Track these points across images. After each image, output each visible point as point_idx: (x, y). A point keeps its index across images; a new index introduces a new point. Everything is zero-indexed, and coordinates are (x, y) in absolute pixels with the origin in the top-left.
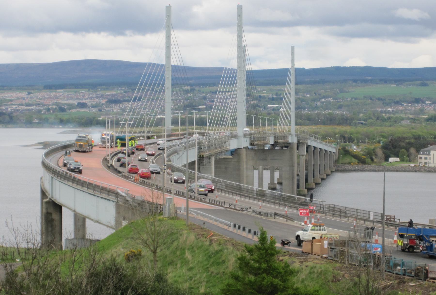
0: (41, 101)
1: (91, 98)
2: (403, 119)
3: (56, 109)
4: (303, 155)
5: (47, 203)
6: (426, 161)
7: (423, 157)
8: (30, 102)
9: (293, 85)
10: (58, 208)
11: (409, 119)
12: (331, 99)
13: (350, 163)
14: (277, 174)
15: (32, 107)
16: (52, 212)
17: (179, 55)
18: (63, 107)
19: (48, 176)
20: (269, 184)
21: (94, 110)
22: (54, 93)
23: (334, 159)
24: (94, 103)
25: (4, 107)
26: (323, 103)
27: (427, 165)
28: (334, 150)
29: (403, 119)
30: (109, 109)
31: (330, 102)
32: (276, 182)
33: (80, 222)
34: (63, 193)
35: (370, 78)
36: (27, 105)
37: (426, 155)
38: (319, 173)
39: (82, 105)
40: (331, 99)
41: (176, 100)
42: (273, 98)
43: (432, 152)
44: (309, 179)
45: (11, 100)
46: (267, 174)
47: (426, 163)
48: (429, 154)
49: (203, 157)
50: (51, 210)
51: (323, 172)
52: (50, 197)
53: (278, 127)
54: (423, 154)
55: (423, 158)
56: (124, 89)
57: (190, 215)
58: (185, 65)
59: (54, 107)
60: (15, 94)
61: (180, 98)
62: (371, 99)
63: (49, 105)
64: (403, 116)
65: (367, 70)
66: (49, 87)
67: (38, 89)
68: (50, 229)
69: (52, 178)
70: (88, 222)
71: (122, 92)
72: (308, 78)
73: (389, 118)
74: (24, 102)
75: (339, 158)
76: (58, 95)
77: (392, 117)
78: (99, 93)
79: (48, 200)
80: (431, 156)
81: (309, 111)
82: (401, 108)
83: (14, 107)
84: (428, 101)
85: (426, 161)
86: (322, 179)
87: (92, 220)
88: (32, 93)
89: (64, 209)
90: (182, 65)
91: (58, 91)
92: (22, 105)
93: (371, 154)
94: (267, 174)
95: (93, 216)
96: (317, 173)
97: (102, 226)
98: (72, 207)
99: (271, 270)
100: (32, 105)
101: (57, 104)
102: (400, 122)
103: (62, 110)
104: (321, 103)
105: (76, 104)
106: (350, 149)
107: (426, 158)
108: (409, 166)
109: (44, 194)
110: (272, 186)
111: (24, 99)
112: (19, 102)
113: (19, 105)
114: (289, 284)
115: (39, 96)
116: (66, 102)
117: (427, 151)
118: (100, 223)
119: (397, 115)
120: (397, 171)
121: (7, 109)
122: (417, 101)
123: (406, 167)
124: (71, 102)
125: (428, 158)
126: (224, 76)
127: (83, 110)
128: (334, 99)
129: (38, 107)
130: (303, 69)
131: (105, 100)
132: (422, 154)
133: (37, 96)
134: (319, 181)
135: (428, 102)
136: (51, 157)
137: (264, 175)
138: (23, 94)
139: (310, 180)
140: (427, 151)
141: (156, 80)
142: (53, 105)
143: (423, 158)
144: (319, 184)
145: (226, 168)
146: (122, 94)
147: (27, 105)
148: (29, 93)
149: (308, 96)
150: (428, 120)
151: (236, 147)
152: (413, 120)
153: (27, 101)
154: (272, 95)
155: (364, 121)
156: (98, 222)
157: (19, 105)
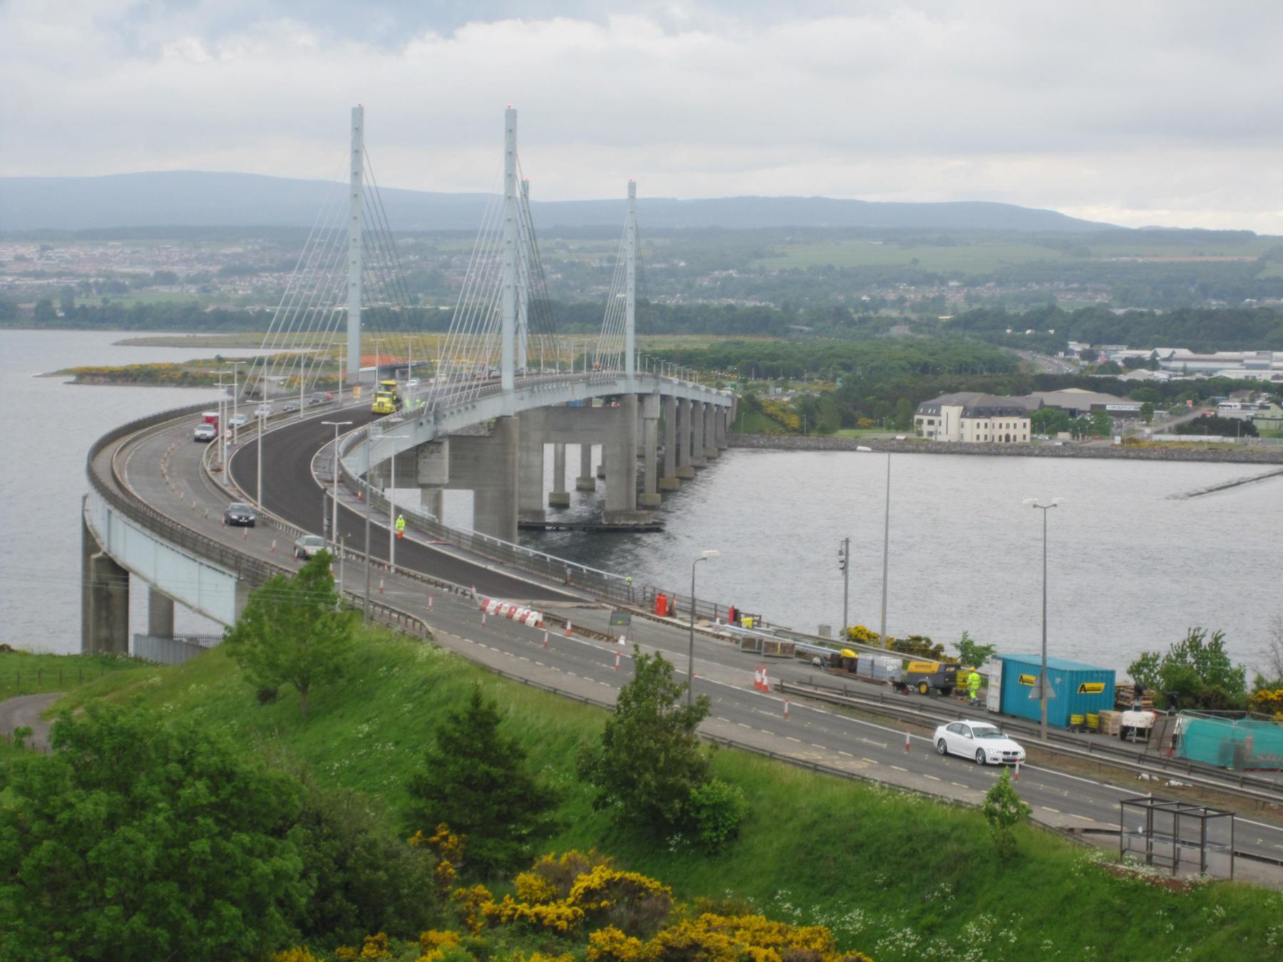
1: (186, 261)
2: (893, 322)
4: (653, 419)
5: (98, 560)
6: (931, 428)
7: (926, 419)
10: (122, 574)
11: (907, 321)
12: (733, 273)
14: (597, 453)
16: (106, 583)
18: (121, 281)
19: (98, 507)
20: (578, 479)
21: (193, 290)
22: (101, 250)
23: (728, 423)
24: (193, 272)
27: (933, 438)
30: (229, 287)
31: (730, 275)
32: (594, 474)
33: (163, 606)
34: (133, 547)
36: (38, 275)
37: (931, 414)
38: (692, 454)
39: (168, 279)
40: (733, 273)
41: (381, 269)
44: (667, 469)
46: (573, 452)
47: (931, 434)
48: (938, 414)
50: (106, 575)
51: (699, 451)
52: (104, 548)
54: (925, 413)
55: (925, 422)
56: (261, 240)
61: (390, 264)
63: (88, 276)
64: (894, 314)
68: (104, 614)
69: (110, 512)
70: (177, 607)
71: (257, 248)
73: (863, 321)
74: (31, 269)
75: (738, 419)
76: (110, 252)
77: (870, 319)
78: (205, 251)
79: (100, 554)
80: (943, 418)
83: (10, 279)
84: (953, 279)
85: (931, 428)
87: (190, 607)
89: (132, 578)
91: (111, 243)
94: (573, 452)
95: (192, 600)
96: (685, 450)
97: (209, 621)
98: (150, 575)
99: (490, 753)
100: (51, 276)
101: (109, 275)
103: (119, 289)
105: (152, 274)
106: (761, 397)
107: (931, 423)
109: (90, 542)
110: (586, 484)
114: (518, 773)
115: (67, 256)
118: (205, 615)
119: (884, 312)
122: (930, 279)
123: (886, 441)
124: (139, 270)
125: (936, 423)
126: (459, 311)
128: (740, 272)
129: (65, 281)
131: (219, 267)
132: (924, 414)
135: (953, 284)
137: (567, 456)
138: (30, 250)
139: (670, 471)
140: (932, 406)
142: (99, 276)
143: (925, 422)
147: (38, 275)
148: (44, 248)
149: (682, 264)
150: (951, 325)
151: (498, 414)
152: (916, 326)
154: (601, 260)
155: (807, 325)
156: (200, 612)
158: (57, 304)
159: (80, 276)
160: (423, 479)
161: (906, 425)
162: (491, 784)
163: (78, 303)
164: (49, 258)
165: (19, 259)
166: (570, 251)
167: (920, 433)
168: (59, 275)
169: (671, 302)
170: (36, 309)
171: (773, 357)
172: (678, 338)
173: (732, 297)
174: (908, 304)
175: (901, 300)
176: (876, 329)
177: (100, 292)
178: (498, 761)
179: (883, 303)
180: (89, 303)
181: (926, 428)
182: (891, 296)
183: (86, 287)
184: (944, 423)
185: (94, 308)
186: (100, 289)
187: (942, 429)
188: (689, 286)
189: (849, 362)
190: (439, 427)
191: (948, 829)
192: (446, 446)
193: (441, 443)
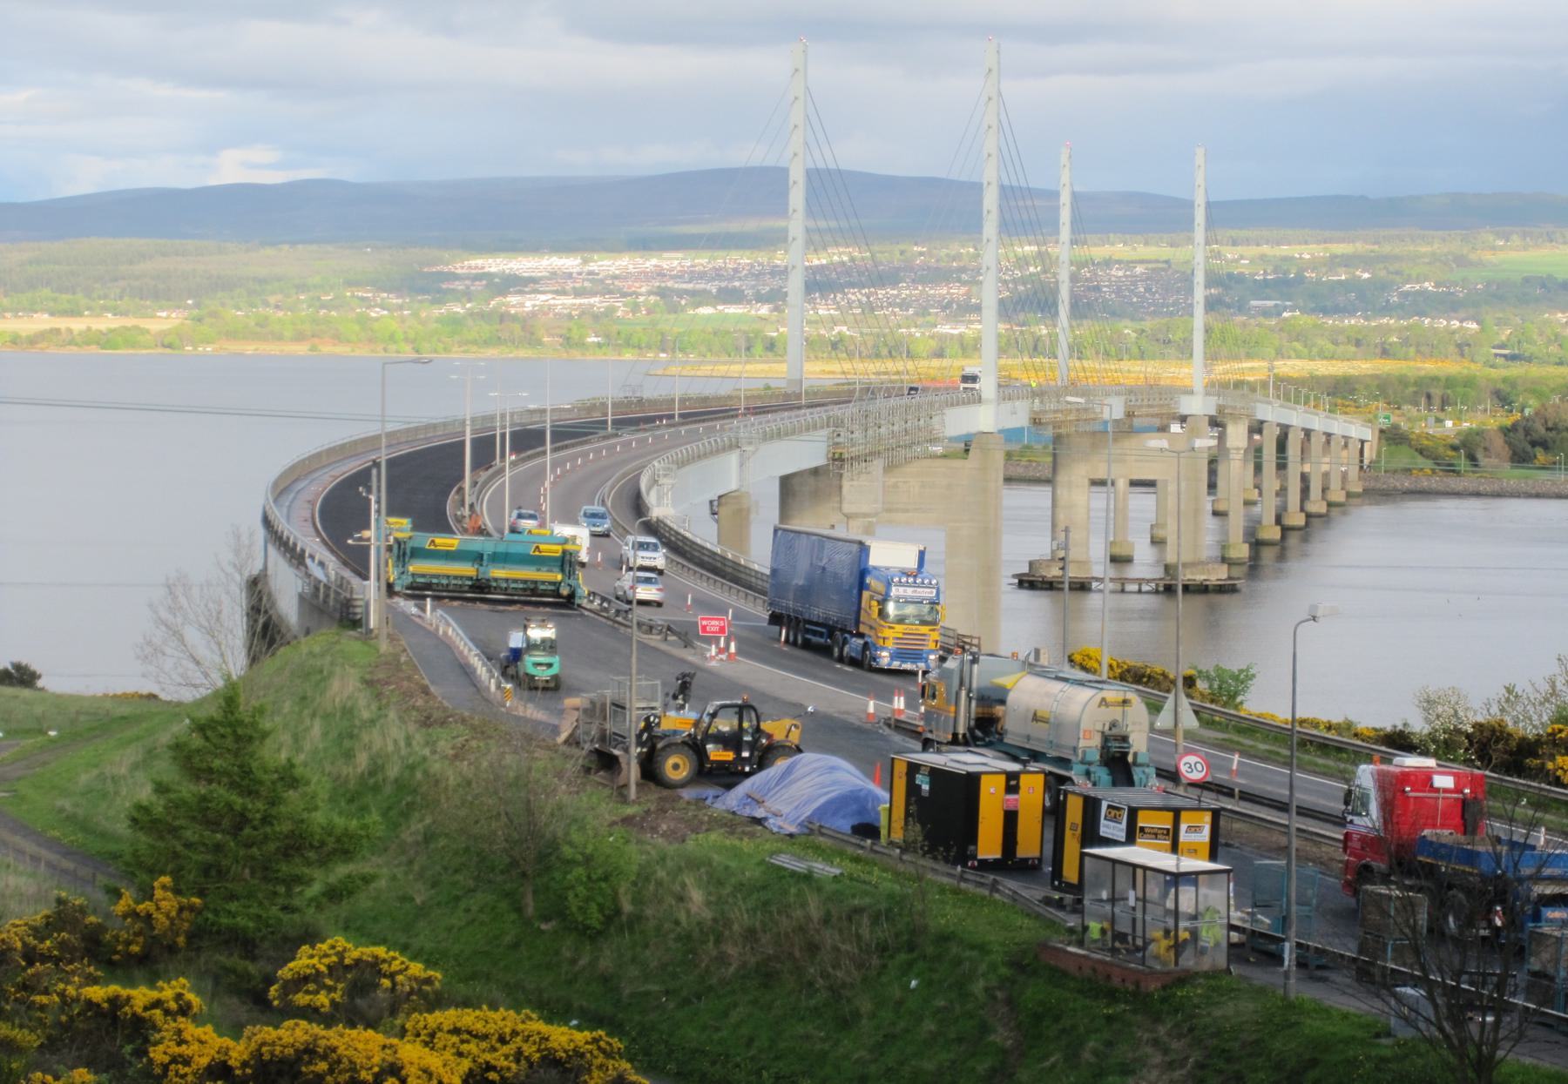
3: (656, 304)
13: (1409, 470)
15: (592, 300)
17: (1014, 153)
26: (1406, 295)
49: (841, 459)
57: (1357, 488)
58: (843, 167)
59: (652, 298)
62: (1543, 286)
81: (1366, 319)
90: (832, 166)
91: (666, 255)
92: (563, 293)
93: (1469, 448)
113: (557, 292)
116: (685, 286)
120: (1538, 496)
121: (522, 305)
127: (733, 310)
136: (1187, 382)
142: (650, 293)
148: (585, 262)
178: (245, 782)
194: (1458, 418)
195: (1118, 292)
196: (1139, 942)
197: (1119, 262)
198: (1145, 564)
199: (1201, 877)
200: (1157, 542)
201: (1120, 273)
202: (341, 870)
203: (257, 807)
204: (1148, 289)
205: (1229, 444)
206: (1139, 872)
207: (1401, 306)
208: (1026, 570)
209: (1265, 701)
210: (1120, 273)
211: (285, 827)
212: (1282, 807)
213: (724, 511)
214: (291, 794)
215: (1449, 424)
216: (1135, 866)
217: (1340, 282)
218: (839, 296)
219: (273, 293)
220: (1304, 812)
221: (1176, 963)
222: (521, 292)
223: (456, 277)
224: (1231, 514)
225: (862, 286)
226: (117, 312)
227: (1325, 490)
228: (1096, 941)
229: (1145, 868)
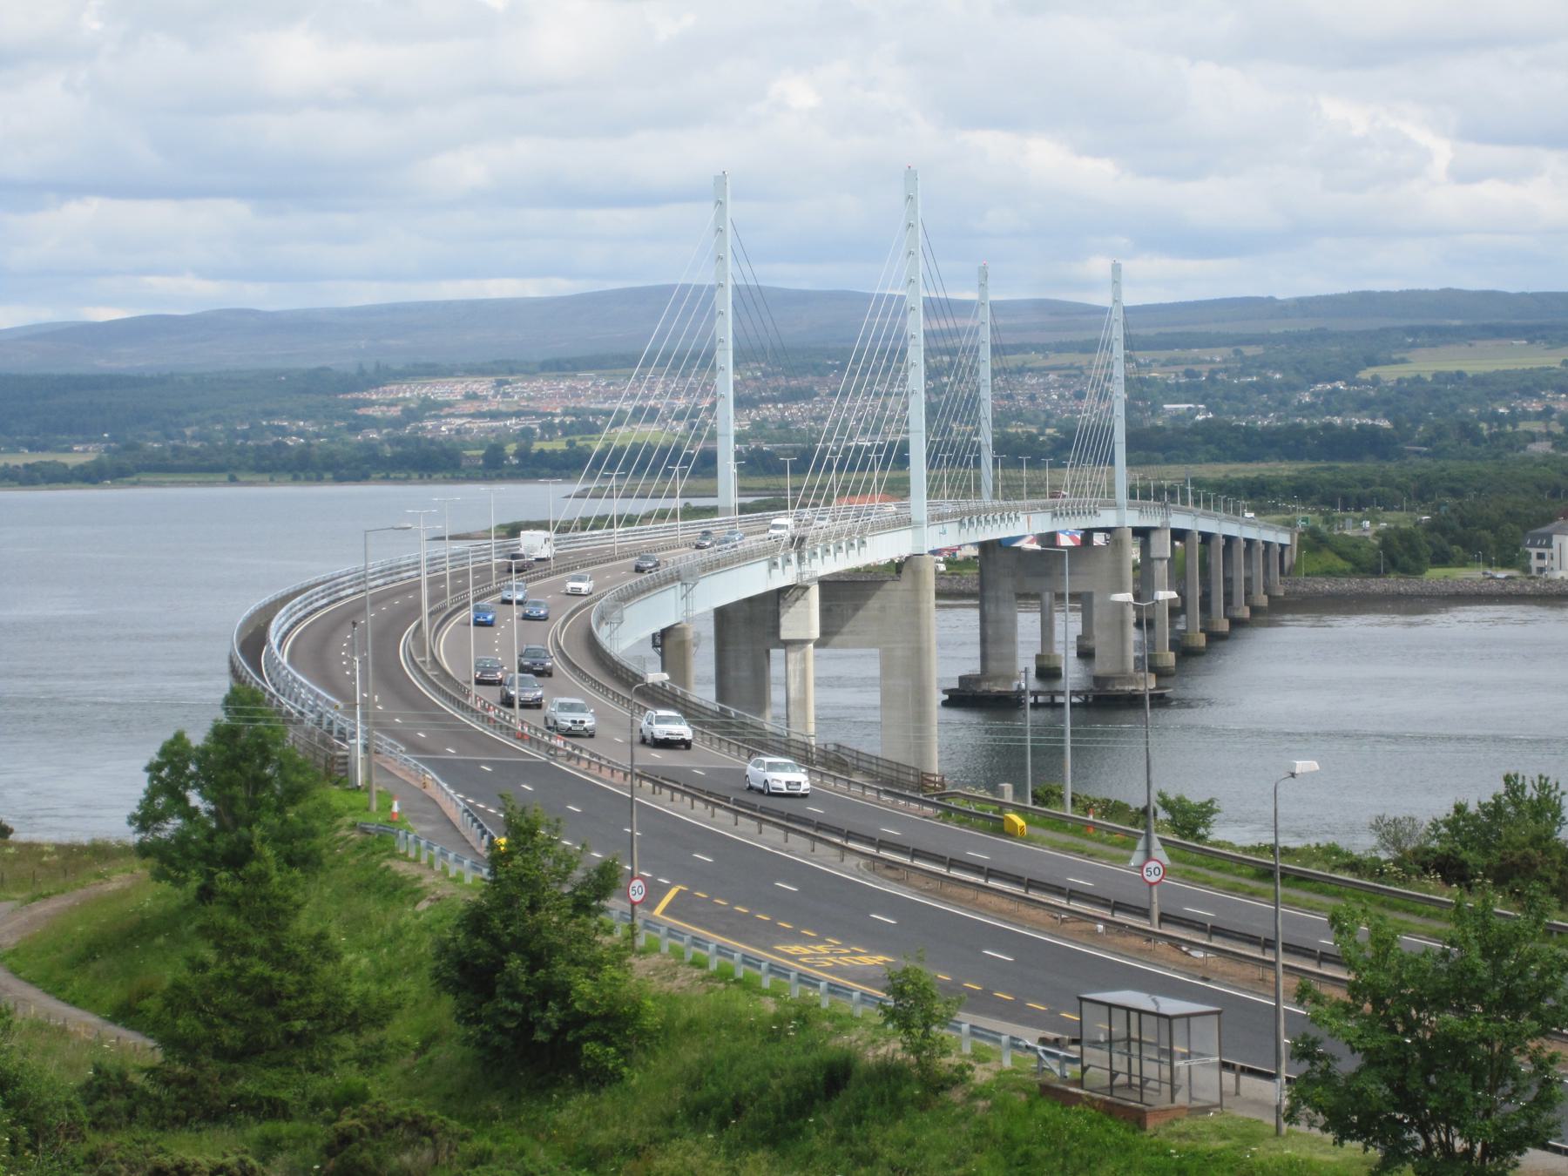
0: (531, 404)
2: (1533, 438)
4: (1161, 559)
6: (1541, 563)
7: (1534, 551)
8: (503, 408)
9: (1119, 351)
21: (680, 428)
25: (429, 424)
28: (1284, 538)
29: (1533, 438)
31: (1335, 391)
35: (1457, 322)
36: (494, 416)
37: (1541, 546)
40: (1341, 386)
42: (1177, 384)
43: (1556, 539)
45: (449, 404)
47: (1541, 570)
48: (1549, 546)
53: (1025, 473)
55: (1534, 556)
60: (459, 387)
63: (554, 415)
64: (1537, 427)
65: (1449, 300)
66: (559, 366)
67: (526, 372)
72: (1157, 331)
73: (1494, 437)
74: (485, 408)
82: (1535, 406)
83: (459, 421)
85: (1541, 563)
86: (1236, 623)
88: (507, 383)
90: (752, 283)
100: (509, 415)
101: (576, 412)
102: (1524, 448)
104: (1313, 394)
107: (1541, 556)
108: (1493, 578)
111: (485, 398)
112: (470, 407)
113: (473, 416)
117: (1542, 536)
119: (1523, 426)
130: (1271, 300)
133: (522, 391)
134: (1224, 626)
138: (483, 386)
141: (876, 339)
142: (565, 414)
143: (1534, 556)
144: (1222, 637)
145: (883, 609)
146: (756, 379)
147: (494, 416)
148: (500, 383)
153: (497, 404)
157: (473, 416)
158: (511, 448)
159: (545, 415)
160: (785, 634)
161: (1510, 557)
162: (269, 997)
163: (537, 446)
164: (506, 395)
165: (471, 397)
166: (1138, 365)
167: (1527, 570)
168: (518, 414)
169: (1262, 423)
170: (485, 457)
171: (1366, 483)
172: (1262, 466)
173: (1338, 414)
174: (1555, 416)
175: (1547, 414)
176: (1510, 446)
177: (565, 434)
178: (280, 956)
179: (1525, 416)
180: (548, 446)
181: (1535, 563)
182: (1535, 406)
183: (549, 428)
184: (1556, 556)
185: (554, 452)
186: (567, 430)
187: (1555, 563)
188: (1284, 403)
189: (1459, 486)
190: (805, 568)
191: (1359, 1056)
192: (814, 593)
193: (806, 588)
194: (1375, 521)
195: (1032, 398)
196: (1136, 1081)
197: (1031, 370)
198: (1073, 674)
199: (1192, 1020)
200: (1085, 654)
201: (1034, 381)
202: (372, 1036)
203: (291, 980)
204: (1061, 396)
205: (1153, 554)
206: (1134, 1016)
207: (1311, 406)
208: (956, 685)
209: (1230, 833)
210: (1034, 381)
211: (317, 998)
212: (1268, 944)
213: (669, 643)
214: (329, 968)
215: (1367, 524)
216: (1129, 1010)
217: (1251, 384)
218: (754, 412)
219: (189, 425)
220: (1290, 949)
221: (1173, 1100)
222: (436, 417)
223: (372, 403)
224: (1504, 771)
225: (775, 401)
226: (32, 447)
227: (1248, 594)
228: (186, 787)
229: (1140, 1012)
